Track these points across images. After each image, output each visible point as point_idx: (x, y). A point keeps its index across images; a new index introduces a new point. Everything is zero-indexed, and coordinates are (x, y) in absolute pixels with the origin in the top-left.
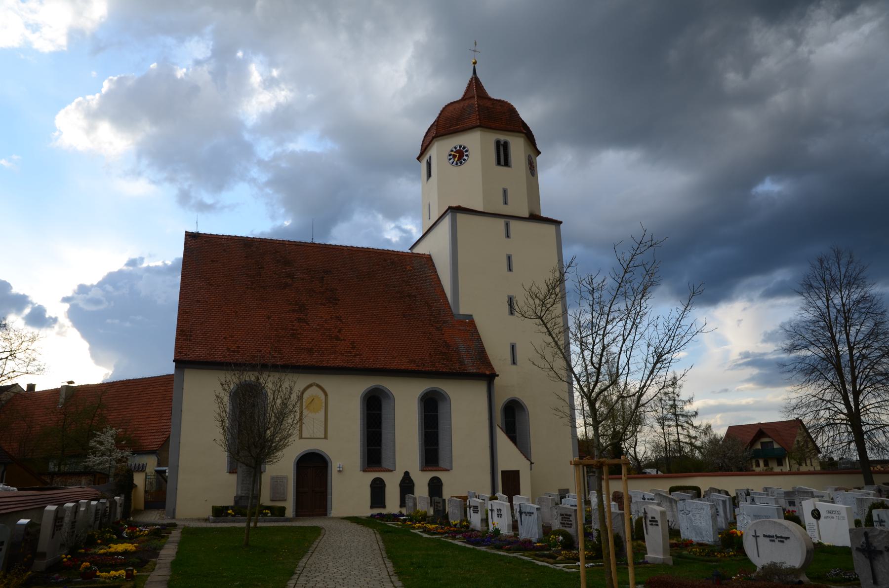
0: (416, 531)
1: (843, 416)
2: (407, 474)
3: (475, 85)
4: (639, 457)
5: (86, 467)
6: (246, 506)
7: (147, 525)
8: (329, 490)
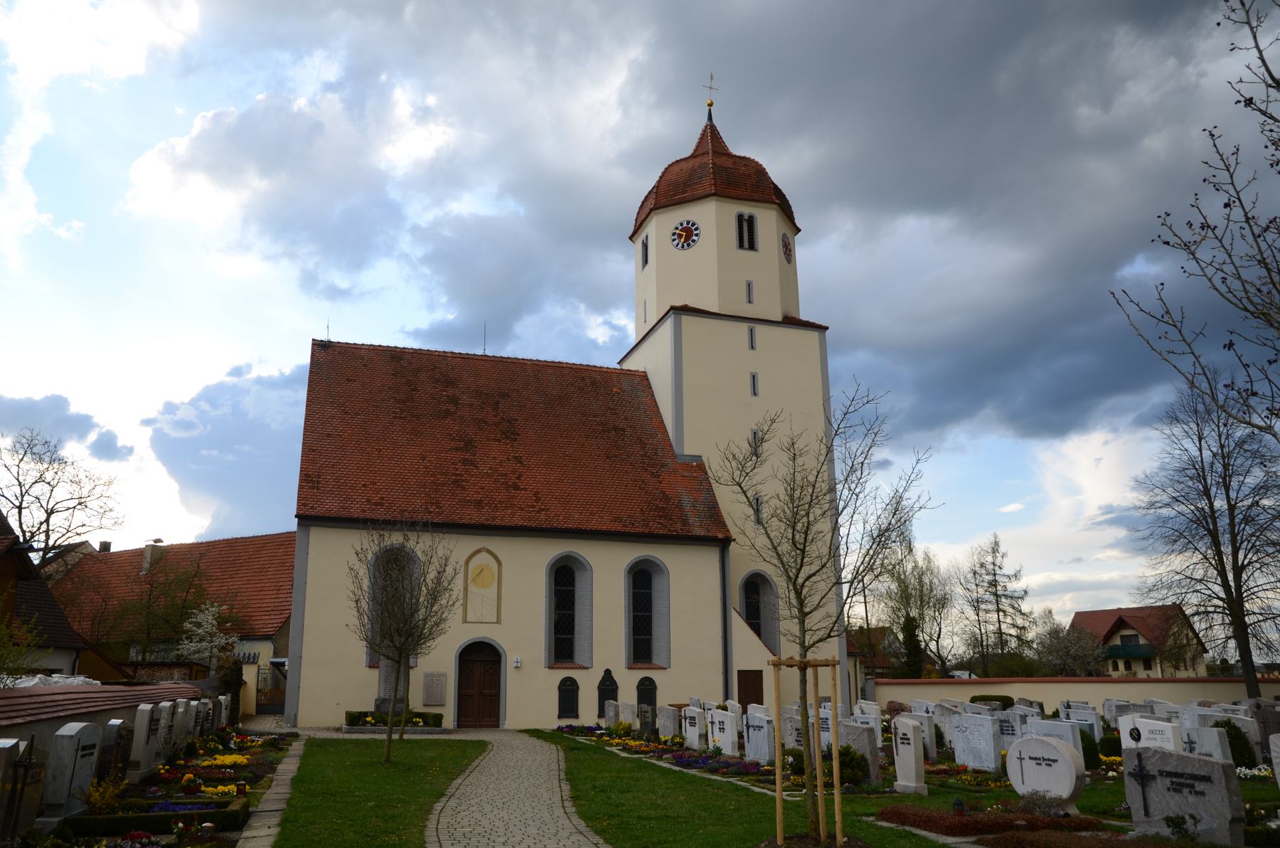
0: (614, 749)
1: (1221, 603)
2: (608, 672)
3: (711, 135)
4: (944, 653)
5: (178, 657)
6: (391, 712)
7: (261, 734)
8: (502, 693)
